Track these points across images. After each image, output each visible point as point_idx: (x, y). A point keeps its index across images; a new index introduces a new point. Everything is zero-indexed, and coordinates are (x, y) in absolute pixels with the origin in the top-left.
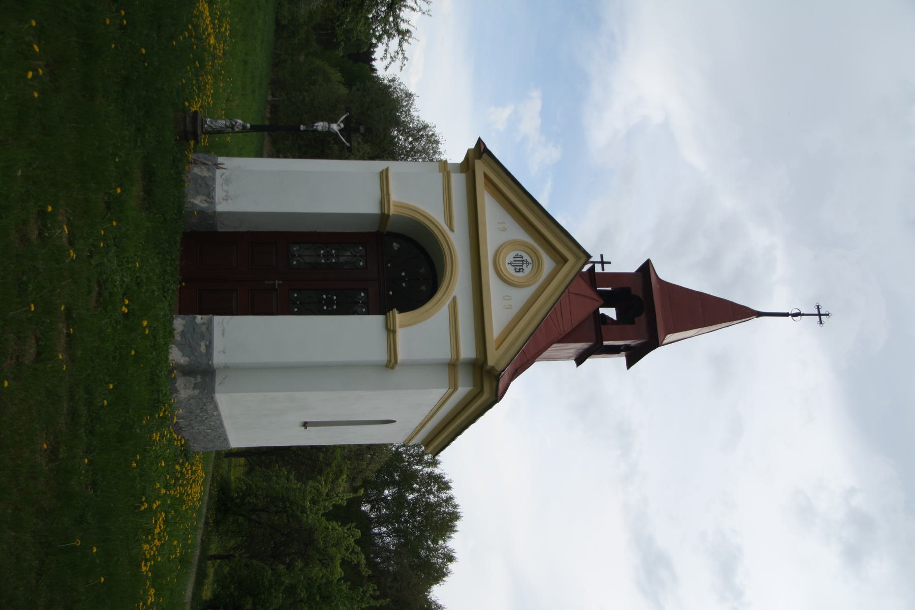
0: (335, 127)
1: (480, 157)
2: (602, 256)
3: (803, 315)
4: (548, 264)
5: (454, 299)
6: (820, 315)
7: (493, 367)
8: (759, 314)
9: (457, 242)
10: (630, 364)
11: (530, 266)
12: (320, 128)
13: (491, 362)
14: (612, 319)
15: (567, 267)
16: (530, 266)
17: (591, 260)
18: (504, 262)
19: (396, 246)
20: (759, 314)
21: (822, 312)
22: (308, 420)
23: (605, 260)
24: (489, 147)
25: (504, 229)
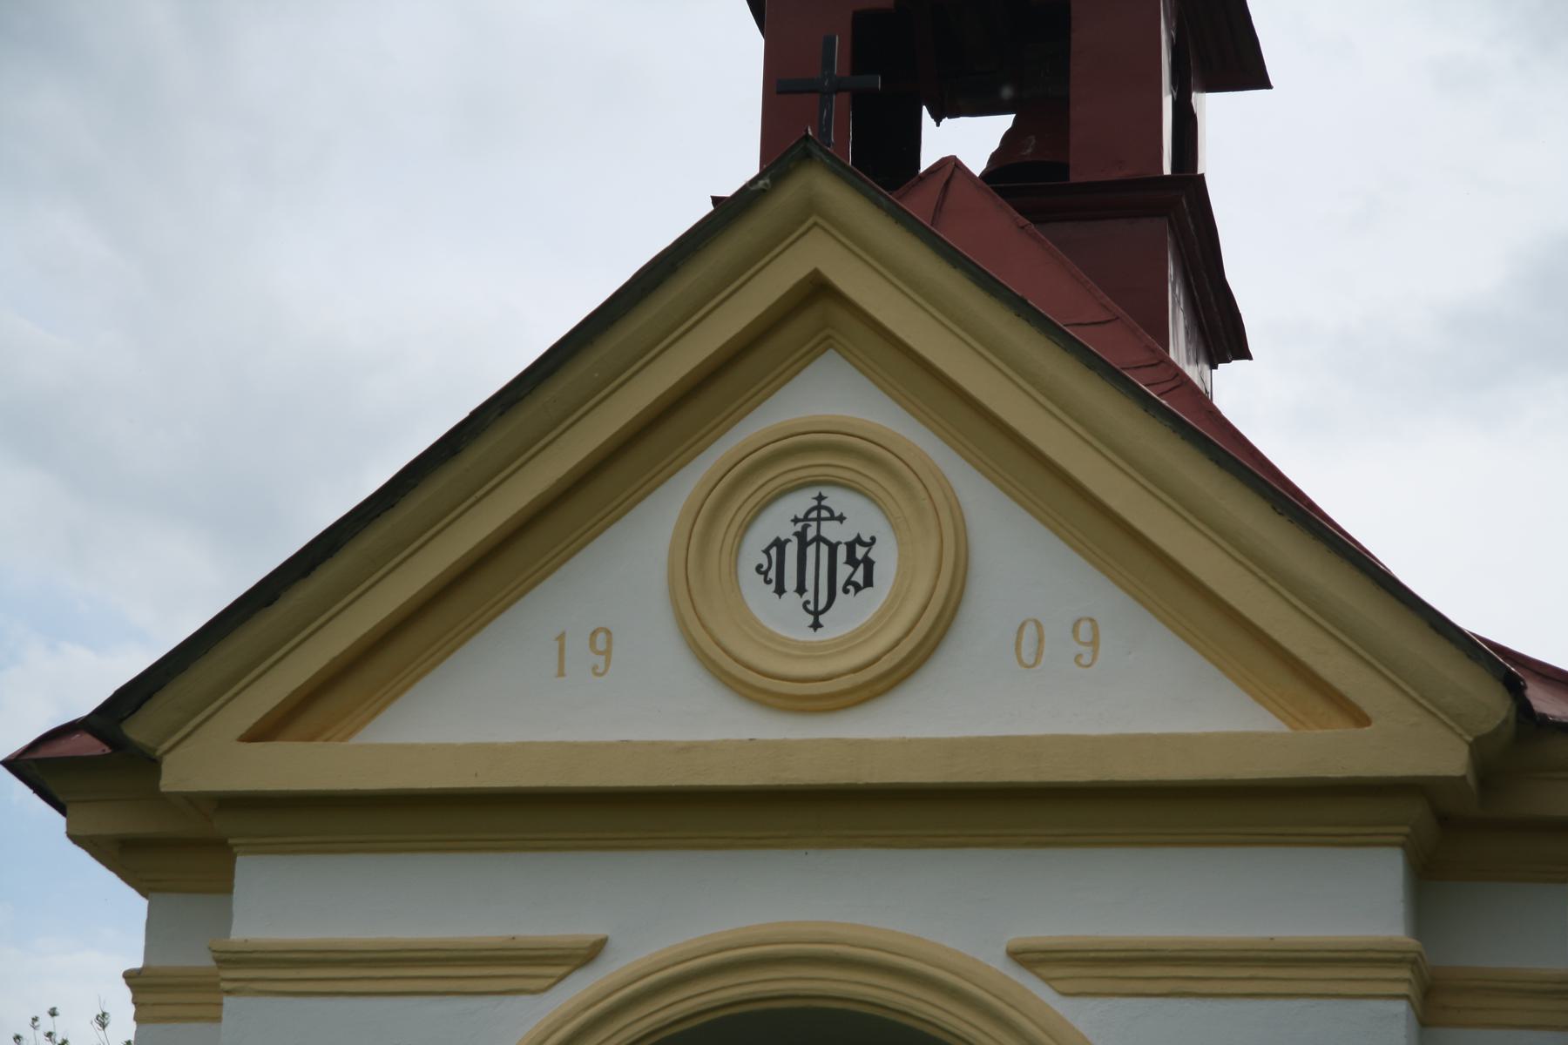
1: (150, 764)
4: (827, 396)
5: (1025, 957)
7: (1478, 747)
11: (837, 500)
13: (1447, 758)
14: (1008, 138)
16: (837, 500)
25: (602, 641)
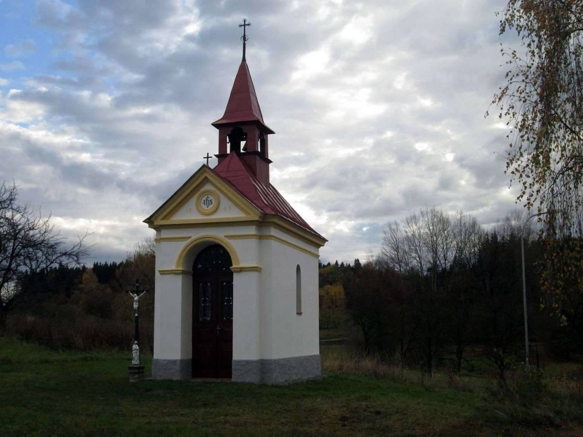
0: (136, 298)
1: (153, 222)
2: (204, 158)
3: (244, 34)
4: (208, 187)
6: (245, 25)
8: (244, 59)
9: (197, 235)
10: (272, 132)
12: (137, 306)
13: (257, 218)
15: (209, 177)
17: (206, 164)
18: (207, 210)
19: (200, 266)
20: (244, 59)
21: (243, 24)
22: (296, 312)
23: (206, 156)
24: (148, 216)
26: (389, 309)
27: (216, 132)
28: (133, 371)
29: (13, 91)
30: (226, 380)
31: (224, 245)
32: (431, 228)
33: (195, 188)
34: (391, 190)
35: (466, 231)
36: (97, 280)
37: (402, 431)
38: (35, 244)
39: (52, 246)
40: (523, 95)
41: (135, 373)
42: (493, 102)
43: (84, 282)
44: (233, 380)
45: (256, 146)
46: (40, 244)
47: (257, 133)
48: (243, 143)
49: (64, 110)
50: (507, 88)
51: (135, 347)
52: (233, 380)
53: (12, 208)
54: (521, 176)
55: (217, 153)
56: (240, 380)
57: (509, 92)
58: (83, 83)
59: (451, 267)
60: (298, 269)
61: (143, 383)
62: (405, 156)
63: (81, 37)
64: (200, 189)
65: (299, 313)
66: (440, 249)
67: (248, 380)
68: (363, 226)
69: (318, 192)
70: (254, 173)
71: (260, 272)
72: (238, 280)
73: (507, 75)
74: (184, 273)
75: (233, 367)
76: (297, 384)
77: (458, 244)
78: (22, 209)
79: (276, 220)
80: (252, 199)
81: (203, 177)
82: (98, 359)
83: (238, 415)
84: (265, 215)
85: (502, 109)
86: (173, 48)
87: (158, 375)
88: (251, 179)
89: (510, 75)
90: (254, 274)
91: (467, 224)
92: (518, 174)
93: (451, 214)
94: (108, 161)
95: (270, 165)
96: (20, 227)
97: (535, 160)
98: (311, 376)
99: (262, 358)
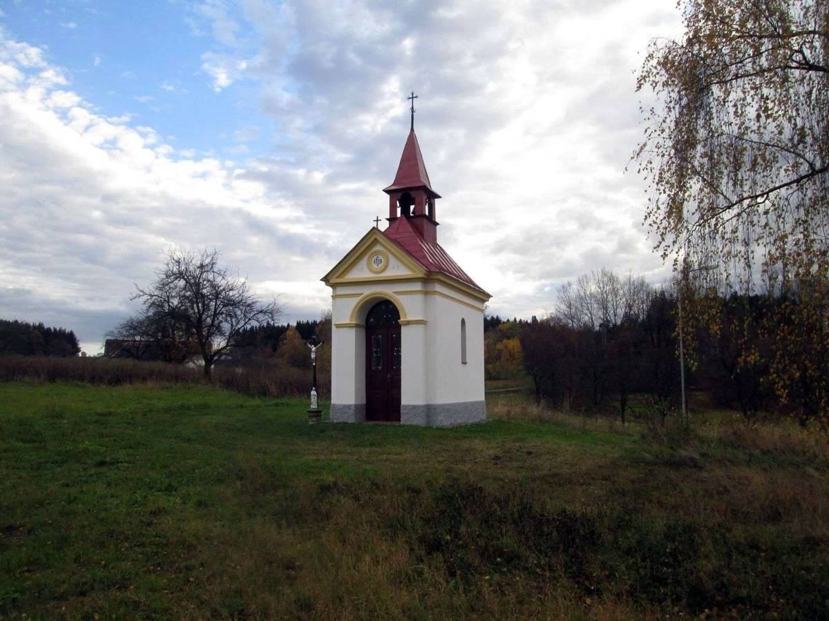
0: (314, 349)
4: (378, 248)
5: (394, 292)
6: (413, 98)
9: (368, 291)
10: (438, 197)
13: (421, 275)
15: (378, 238)
19: (372, 320)
20: (412, 130)
21: (414, 99)
24: (324, 276)
26: (542, 360)
27: (387, 197)
28: (312, 414)
29: (238, 171)
30: (397, 423)
31: (392, 300)
32: (601, 286)
33: (367, 248)
34: (573, 253)
35: (634, 289)
36: (300, 336)
37: (550, 470)
38: (230, 303)
39: (249, 305)
40: (661, 150)
41: (314, 416)
42: (632, 158)
43: (288, 338)
44: (402, 423)
45: (424, 209)
46: (239, 303)
47: (425, 197)
48: (412, 207)
49: (281, 186)
50: (645, 145)
51: (313, 393)
52: (402, 423)
53: (213, 272)
54: (658, 228)
55: (388, 217)
56: (409, 423)
57: (647, 148)
58: (298, 164)
59: (622, 323)
60: (463, 322)
61: (321, 425)
62: (585, 222)
63: (298, 122)
64: (372, 247)
65: (464, 363)
66: (610, 305)
67: (415, 423)
68: (544, 286)
69: (506, 257)
70: (420, 233)
71: (425, 324)
72: (405, 332)
73: (646, 131)
74: (357, 326)
75: (402, 411)
76: (460, 427)
77: (627, 300)
78: (222, 273)
79: (440, 277)
80: (418, 258)
81: (372, 239)
82: (288, 405)
83: (400, 454)
84: (429, 273)
85: (640, 164)
86: (379, 129)
87: (336, 418)
88: (418, 240)
89: (649, 132)
90: (420, 328)
91: (636, 283)
92: (655, 226)
93: (622, 274)
94: (317, 232)
95: (438, 227)
96: (221, 288)
97: (669, 214)
98: (477, 420)
99: (430, 403)
